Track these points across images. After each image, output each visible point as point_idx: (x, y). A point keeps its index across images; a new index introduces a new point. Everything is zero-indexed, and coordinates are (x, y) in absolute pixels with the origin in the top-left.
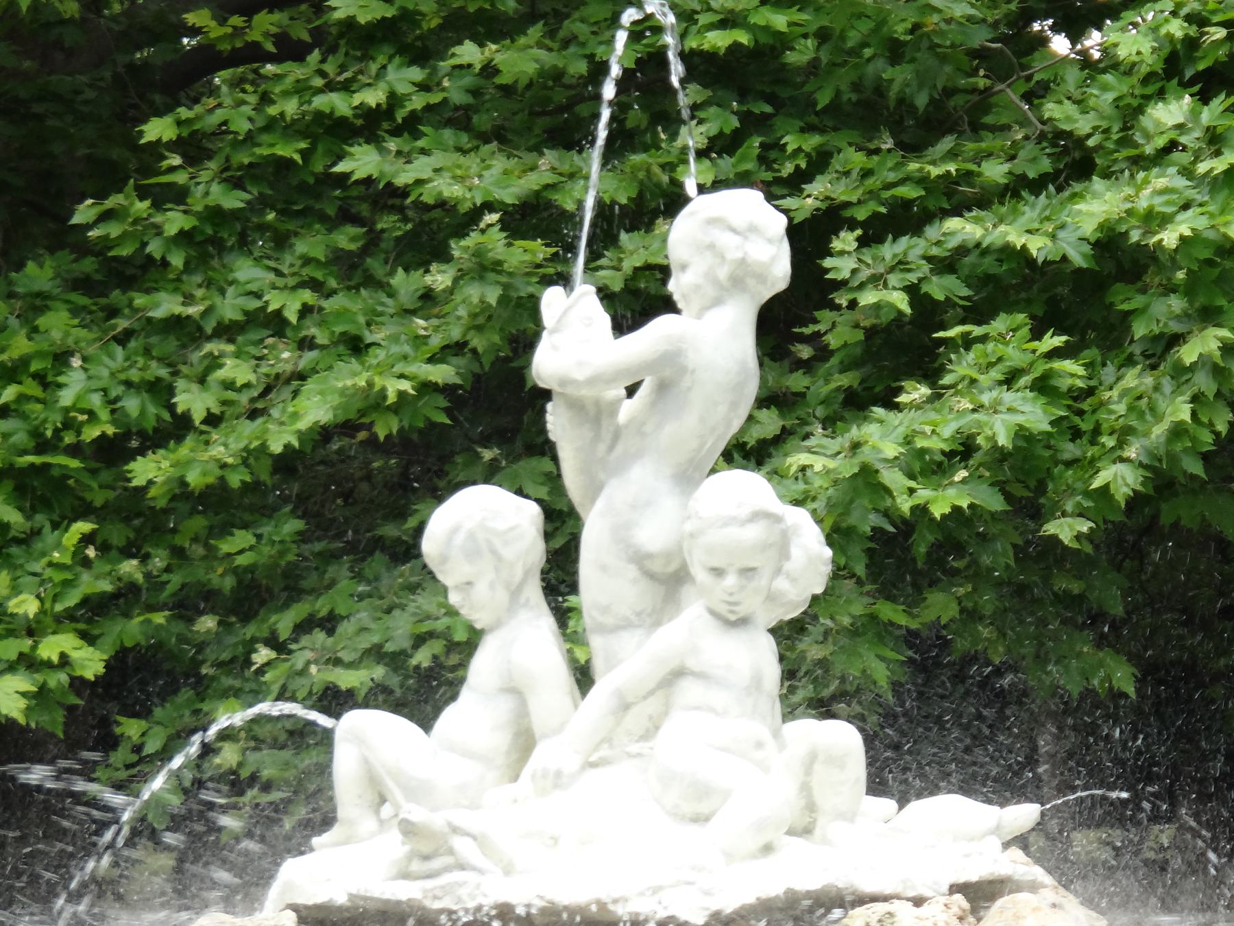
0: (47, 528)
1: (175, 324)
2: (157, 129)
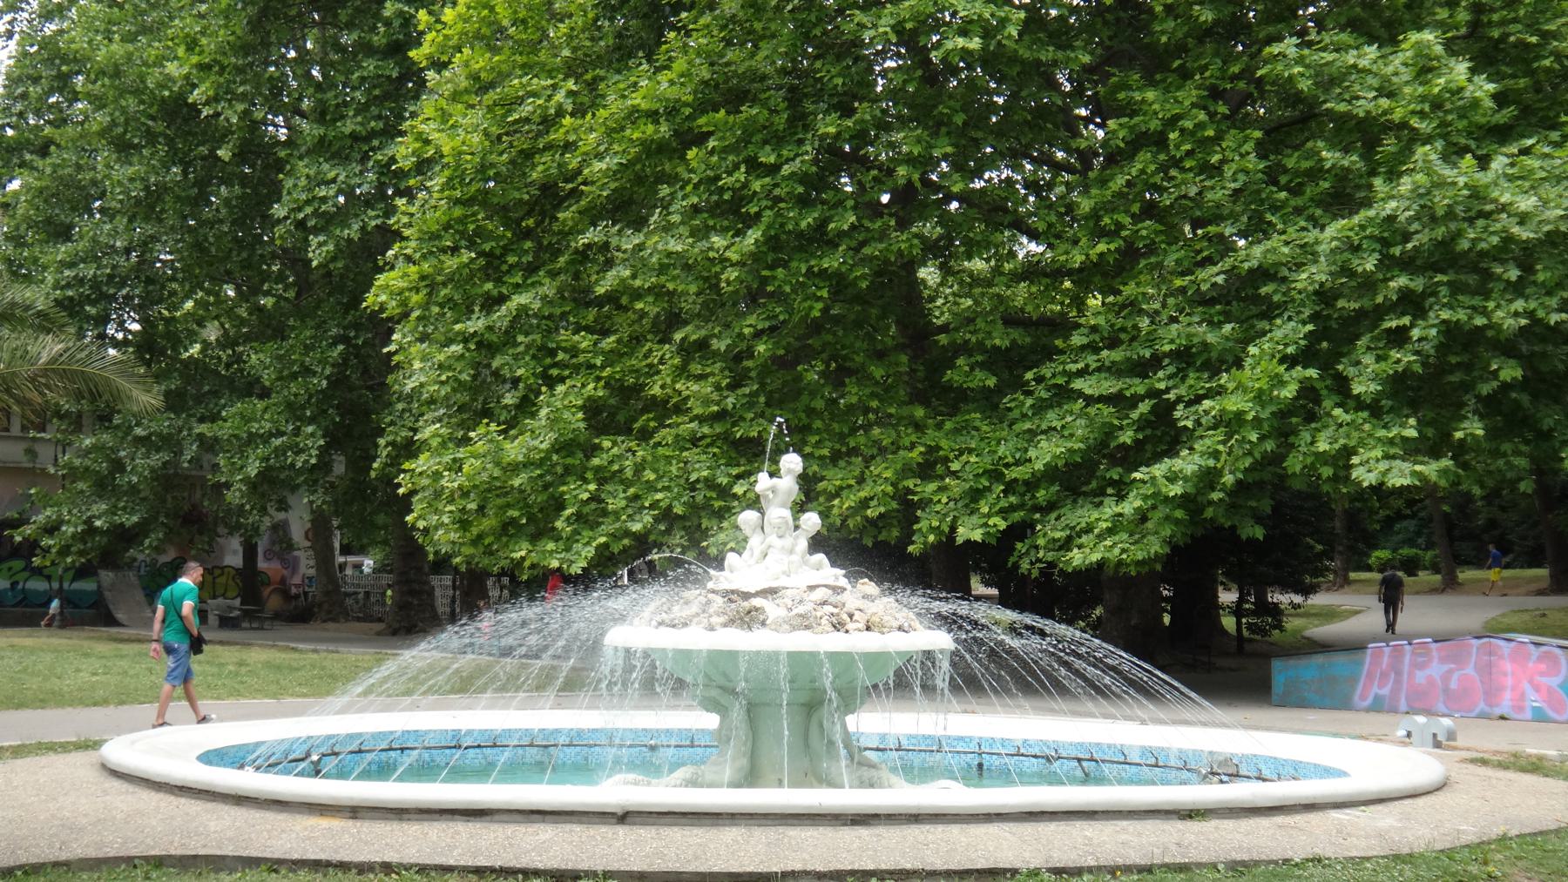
0: (281, 516)
1: (1030, 431)
2: (1029, 375)
